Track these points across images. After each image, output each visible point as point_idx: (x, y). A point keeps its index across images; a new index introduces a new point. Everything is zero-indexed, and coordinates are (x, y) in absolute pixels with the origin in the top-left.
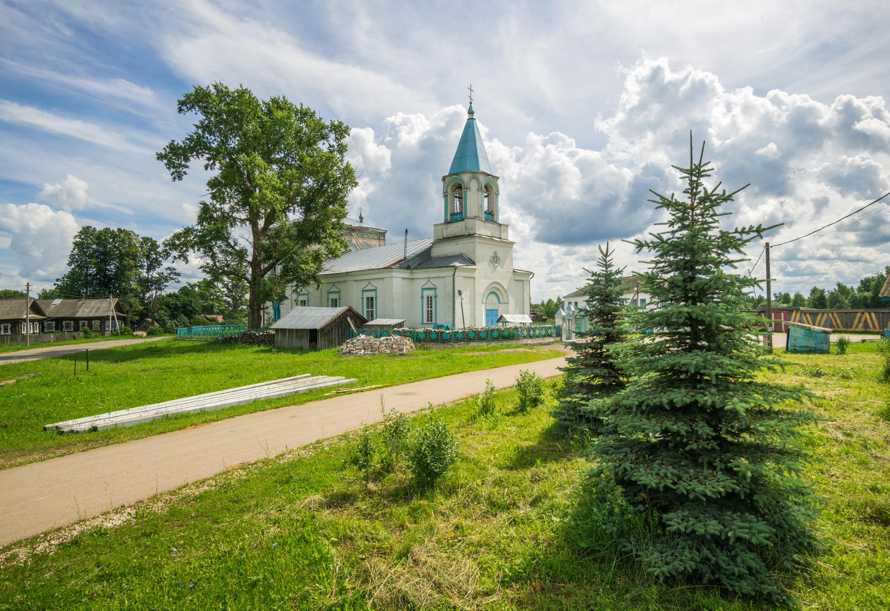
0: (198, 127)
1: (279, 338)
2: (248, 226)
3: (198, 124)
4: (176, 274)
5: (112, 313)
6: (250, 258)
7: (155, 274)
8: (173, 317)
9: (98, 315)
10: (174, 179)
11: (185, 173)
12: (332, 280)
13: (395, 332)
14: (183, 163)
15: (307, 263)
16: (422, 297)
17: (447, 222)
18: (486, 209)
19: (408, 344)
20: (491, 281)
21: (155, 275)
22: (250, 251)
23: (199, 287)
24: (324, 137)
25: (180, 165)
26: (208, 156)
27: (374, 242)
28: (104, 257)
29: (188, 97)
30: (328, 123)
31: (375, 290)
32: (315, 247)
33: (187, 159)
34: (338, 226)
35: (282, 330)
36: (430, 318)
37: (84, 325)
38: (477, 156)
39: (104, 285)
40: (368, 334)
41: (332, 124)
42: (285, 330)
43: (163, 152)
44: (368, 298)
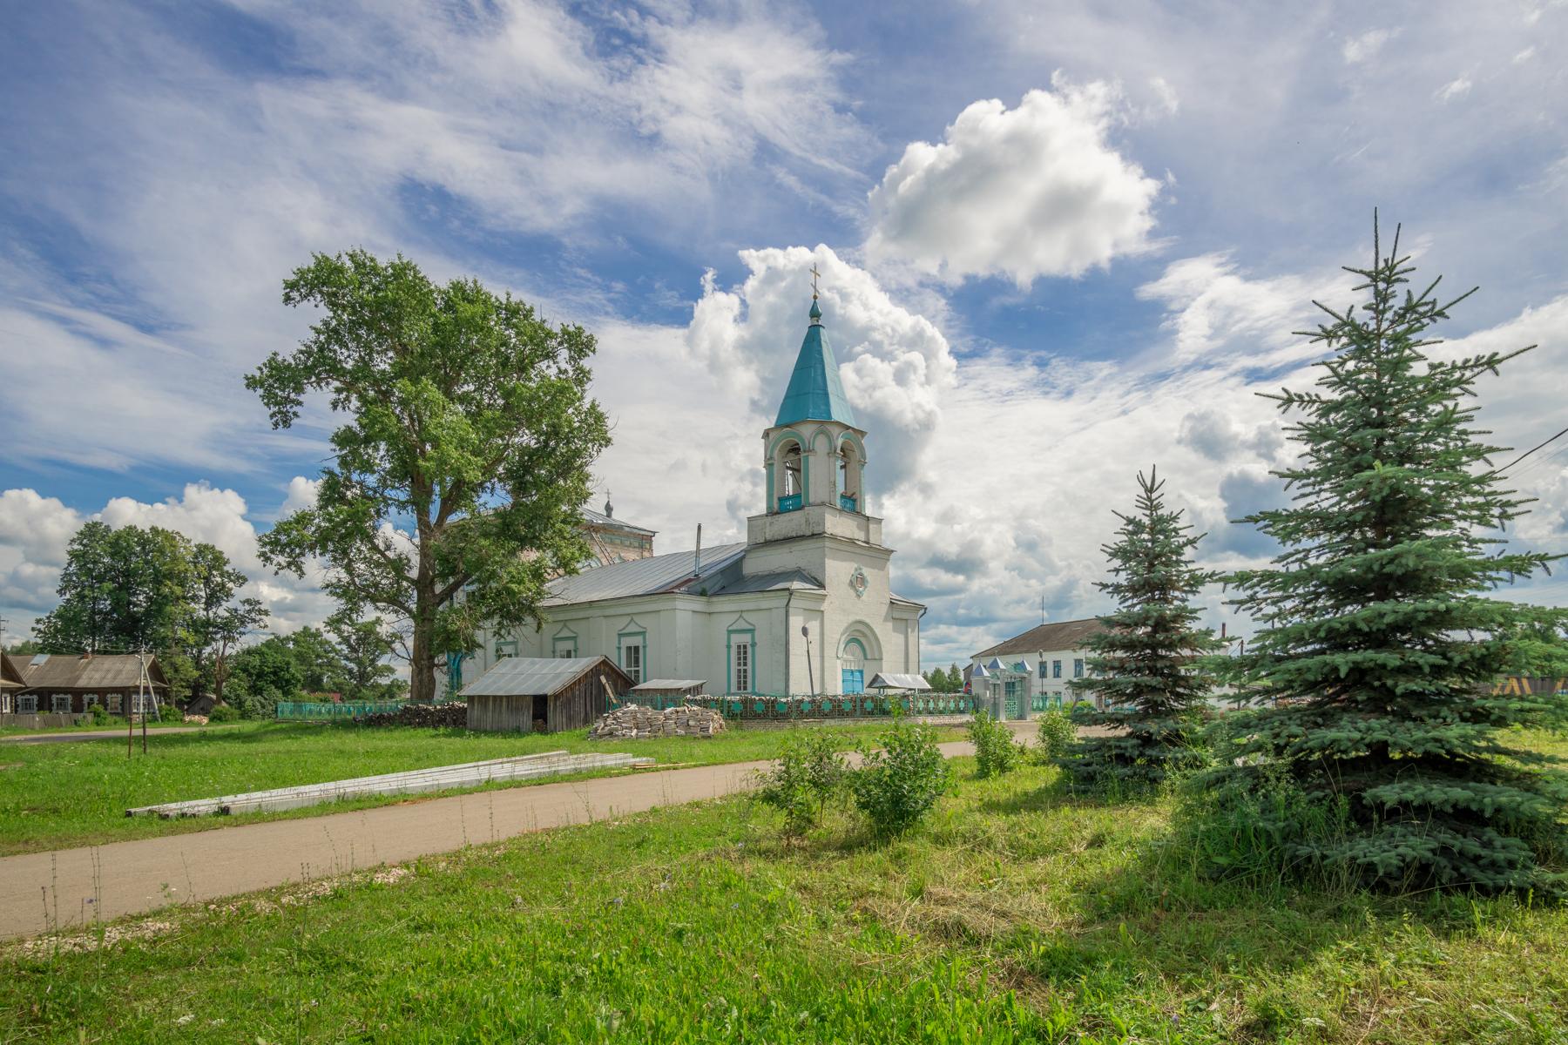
0: (318, 332)
1: (475, 714)
2: (410, 516)
3: (319, 325)
4: (260, 612)
5: (144, 681)
6: (414, 574)
7: (222, 611)
8: (255, 690)
9: (117, 683)
10: (276, 425)
11: (295, 414)
12: (561, 617)
13: (688, 701)
14: (293, 396)
15: (520, 582)
16: (729, 647)
17: (771, 513)
18: (841, 489)
19: (716, 720)
20: (852, 618)
21: (222, 612)
22: (416, 560)
23: (296, 642)
24: (550, 355)
25: (287, 400)
26: (337, 384)
27: (631, 555)
28: (126, 582)
29: (302, 273)
30: (557, 329)
31: (643, 633)
32: (530, 556)
33: (299, 389)
34: (572, 519)
35: (480, 697)
36: (742, 685)
37: (91, 702)
38: (826, 395)
39: (127, 630)
40: (641, 704)
41: (565, 331)
42: (487, 697)
43: (258, 374)
44: (629, 648)
